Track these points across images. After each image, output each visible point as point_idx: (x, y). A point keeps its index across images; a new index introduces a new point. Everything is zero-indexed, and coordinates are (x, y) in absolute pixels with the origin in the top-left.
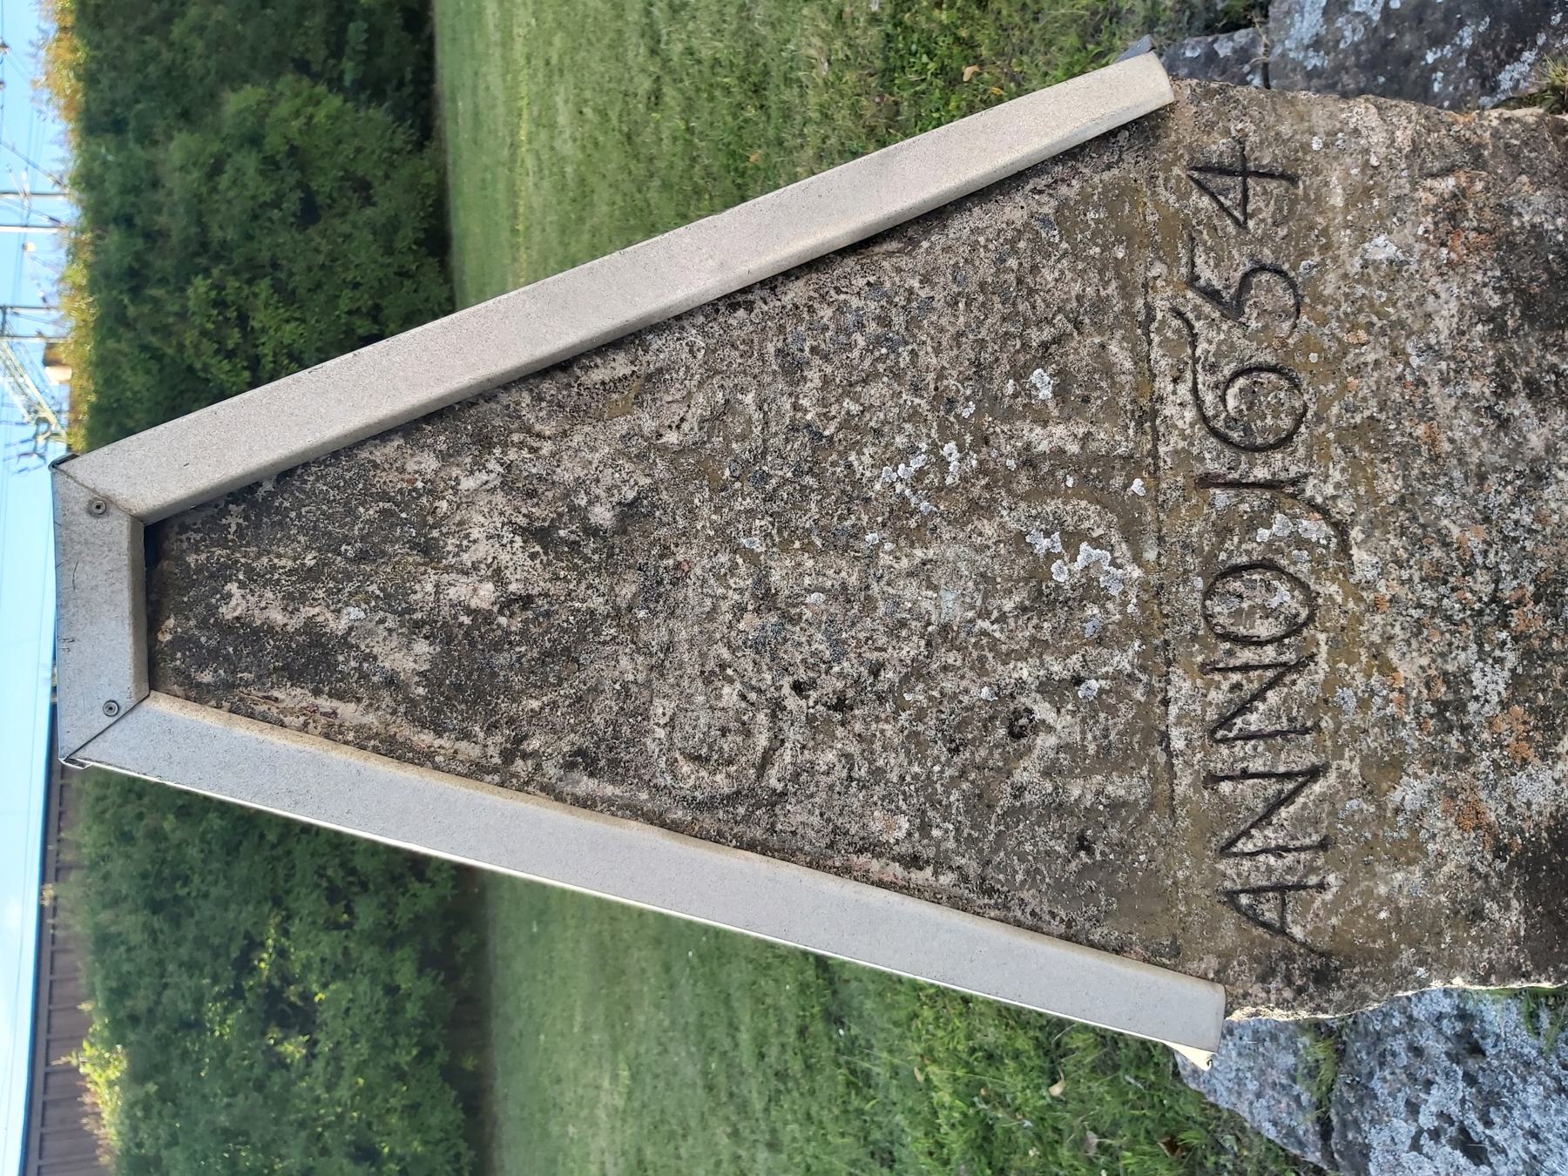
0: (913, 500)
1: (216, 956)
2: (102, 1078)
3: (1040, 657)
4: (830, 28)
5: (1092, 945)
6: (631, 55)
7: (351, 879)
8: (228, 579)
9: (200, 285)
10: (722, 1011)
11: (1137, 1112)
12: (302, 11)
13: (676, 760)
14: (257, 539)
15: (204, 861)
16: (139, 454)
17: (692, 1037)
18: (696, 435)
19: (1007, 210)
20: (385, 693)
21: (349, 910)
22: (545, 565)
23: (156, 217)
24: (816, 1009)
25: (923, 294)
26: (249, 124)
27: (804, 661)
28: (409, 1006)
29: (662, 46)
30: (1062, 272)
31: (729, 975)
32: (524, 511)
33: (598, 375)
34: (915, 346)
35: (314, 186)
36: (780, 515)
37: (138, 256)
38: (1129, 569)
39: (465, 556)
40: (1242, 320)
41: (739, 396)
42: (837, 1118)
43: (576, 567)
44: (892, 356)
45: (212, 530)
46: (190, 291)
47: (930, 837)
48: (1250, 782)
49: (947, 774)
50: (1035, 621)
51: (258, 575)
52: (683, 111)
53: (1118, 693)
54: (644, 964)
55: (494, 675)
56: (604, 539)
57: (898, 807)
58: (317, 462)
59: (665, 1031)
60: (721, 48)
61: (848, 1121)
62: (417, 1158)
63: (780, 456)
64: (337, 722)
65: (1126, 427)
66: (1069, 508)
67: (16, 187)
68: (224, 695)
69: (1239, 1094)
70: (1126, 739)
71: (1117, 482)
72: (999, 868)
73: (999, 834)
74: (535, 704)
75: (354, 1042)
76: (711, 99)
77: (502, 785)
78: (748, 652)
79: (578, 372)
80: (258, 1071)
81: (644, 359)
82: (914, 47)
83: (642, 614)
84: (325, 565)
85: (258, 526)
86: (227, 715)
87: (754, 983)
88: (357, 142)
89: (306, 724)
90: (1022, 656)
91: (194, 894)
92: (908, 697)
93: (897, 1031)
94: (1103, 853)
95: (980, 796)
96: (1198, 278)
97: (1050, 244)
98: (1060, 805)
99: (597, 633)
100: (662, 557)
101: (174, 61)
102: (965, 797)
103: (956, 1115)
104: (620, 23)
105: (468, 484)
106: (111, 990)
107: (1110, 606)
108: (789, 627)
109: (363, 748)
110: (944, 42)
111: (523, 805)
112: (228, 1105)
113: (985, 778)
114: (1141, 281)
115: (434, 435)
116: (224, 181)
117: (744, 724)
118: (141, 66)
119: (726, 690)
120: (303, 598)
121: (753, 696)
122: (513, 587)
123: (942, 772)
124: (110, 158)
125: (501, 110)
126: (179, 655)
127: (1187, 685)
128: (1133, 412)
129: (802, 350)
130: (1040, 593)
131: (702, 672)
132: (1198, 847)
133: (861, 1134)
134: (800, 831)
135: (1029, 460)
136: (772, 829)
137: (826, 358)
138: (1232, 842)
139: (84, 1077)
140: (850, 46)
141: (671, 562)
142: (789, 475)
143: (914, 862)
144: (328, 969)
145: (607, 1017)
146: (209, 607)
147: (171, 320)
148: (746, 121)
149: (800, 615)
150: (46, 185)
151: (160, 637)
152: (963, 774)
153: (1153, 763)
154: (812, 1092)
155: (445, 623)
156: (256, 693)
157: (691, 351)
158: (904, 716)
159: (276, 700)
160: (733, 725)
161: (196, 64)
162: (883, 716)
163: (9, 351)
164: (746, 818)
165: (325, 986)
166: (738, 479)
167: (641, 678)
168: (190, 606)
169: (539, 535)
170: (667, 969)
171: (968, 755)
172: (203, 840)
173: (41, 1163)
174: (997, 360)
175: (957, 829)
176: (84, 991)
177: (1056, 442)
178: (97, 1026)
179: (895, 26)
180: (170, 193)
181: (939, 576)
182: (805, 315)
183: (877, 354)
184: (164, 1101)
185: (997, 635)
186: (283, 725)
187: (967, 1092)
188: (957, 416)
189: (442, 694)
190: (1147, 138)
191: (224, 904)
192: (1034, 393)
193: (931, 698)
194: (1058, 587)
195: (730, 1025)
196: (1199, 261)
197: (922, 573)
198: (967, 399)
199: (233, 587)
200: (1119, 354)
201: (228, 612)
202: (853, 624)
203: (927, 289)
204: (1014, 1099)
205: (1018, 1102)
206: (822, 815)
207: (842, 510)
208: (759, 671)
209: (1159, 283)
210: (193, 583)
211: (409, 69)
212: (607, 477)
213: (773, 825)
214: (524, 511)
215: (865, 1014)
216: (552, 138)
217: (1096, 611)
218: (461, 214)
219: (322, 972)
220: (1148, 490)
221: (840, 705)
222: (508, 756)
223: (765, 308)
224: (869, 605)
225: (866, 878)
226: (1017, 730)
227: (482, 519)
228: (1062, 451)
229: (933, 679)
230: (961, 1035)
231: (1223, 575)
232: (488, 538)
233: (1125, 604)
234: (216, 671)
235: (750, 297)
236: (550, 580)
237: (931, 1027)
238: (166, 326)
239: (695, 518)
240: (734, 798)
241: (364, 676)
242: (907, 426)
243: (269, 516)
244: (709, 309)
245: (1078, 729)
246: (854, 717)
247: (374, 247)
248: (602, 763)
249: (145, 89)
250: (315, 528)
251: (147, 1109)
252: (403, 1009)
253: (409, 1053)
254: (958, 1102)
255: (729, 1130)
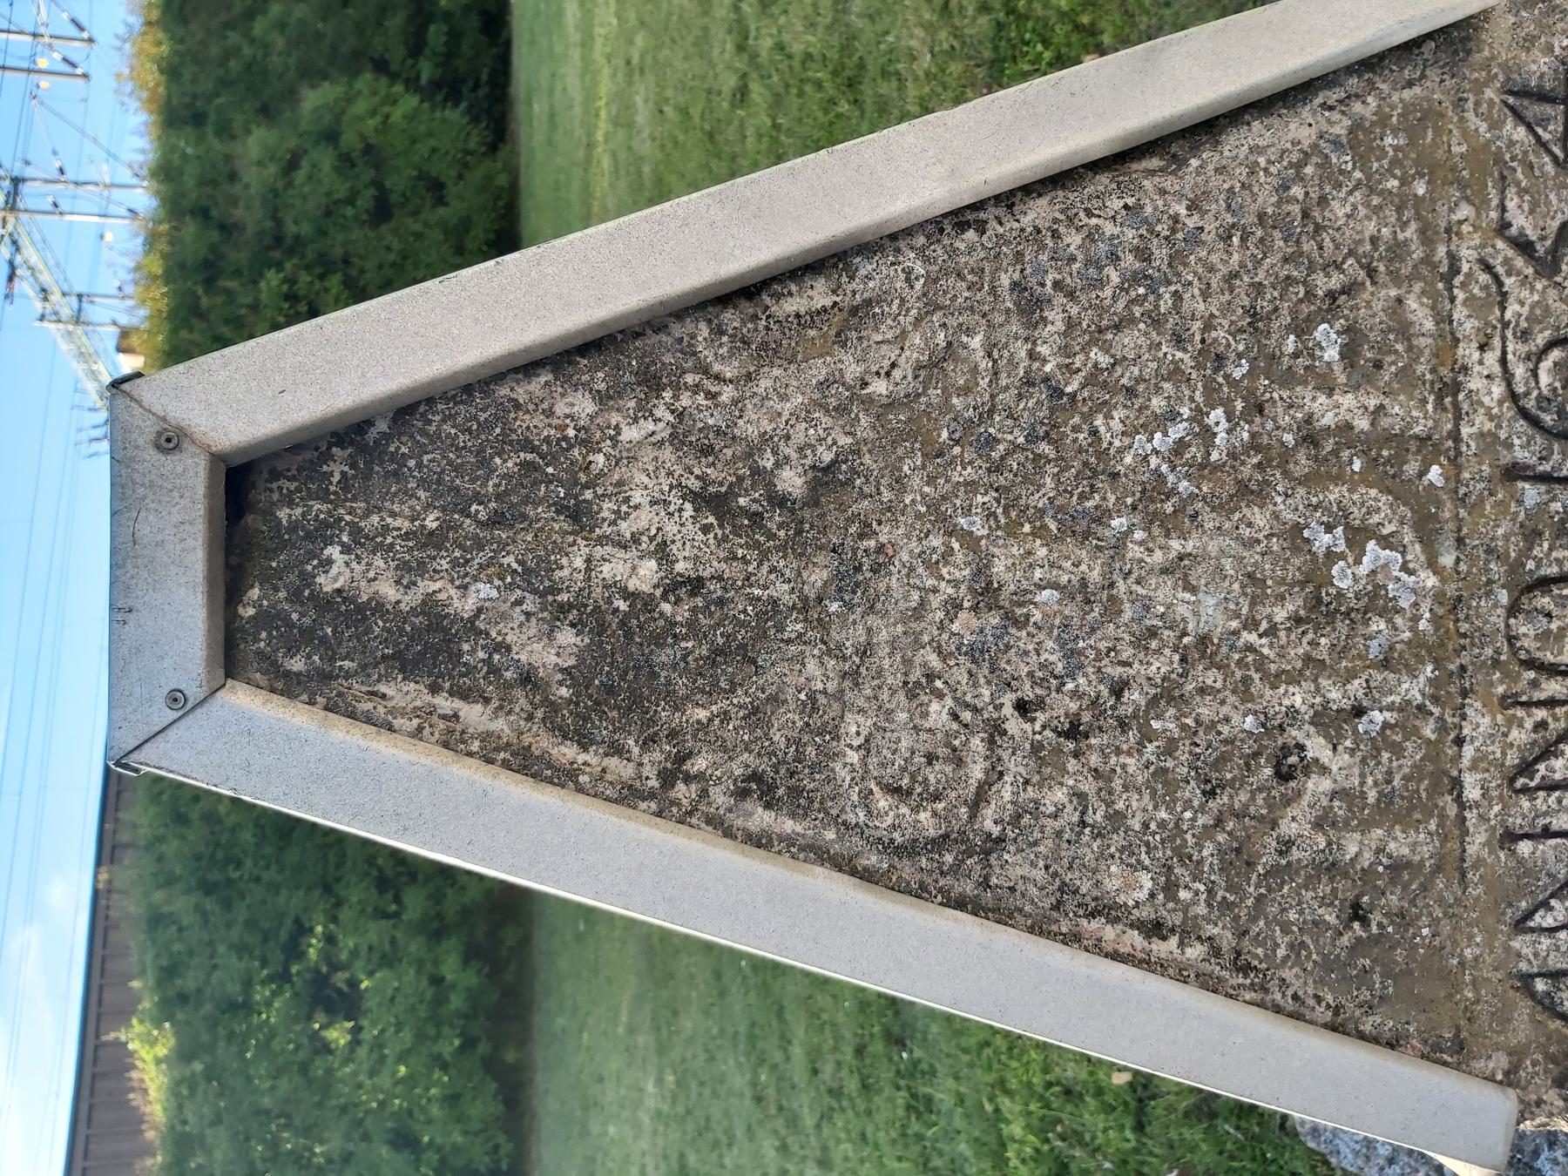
0: (1171, 478)
1: (266, 939)
2: (150, 1054)
3: (1315, 681)
4: (935, 18)
5: (1362, 1036)
6: (716, 51)
7: (400, 869)
8: (329, 541)
9: (272, 279)
10: (774, 1023)
11: (1235, 1164)
12: (383, 11)
13: (871, 792)
14: (366, 494)
15: (257, 845)
16: (223, 375)
17: (742, 1047)
18: (911, 385)
19: (1292, 126)
20: (518, 693)
21: (397, 899)
22: (720, 541)
23: (232, 210)
24: (876, 1029)
25: (1191, 223)
26: (326, 121)
27: (1031, 674)
28: (453, 997)
29: (751, 42)
30: (1354, 207)
31: (783, 987)
32: (697, 471)
33: (791, 306)
34: (1179, 287)
35: (388, 184)
36: (1007, 489)
37: (213, 248)
38: (1423, 575)
39: (623, 525)
40: (1558, 279)
41: (965, 339)
42: (894, 1142)
43: (757, 545)
44: (1151, 298)
45: (310, 479)
46: (263, 285)
47: (1176, 900)
48: (1553, 842)
49: (1200, 822)
50: (1310, 636)
51: (367, 537)
52: (770, 107)
53: (1404, 728)
54: (693, 970)
55: (654, 675)
56: (793, 511)
57: (1139, 861)
58: (445, 397)
59: (714, 1038)
60: (811, 41)
61: (906, 1146)
62: (456, 1149)
63: (1010, 416)
64: (459, 728)
65: (1424, 401)
66: (1355, 497)
67: (96, 178)
68: (314, 687)
69: (1368, 1158)
70: (1412, 786)
71: (1411, 468)
72: (1256, 940)
73: (1260, 899)
74: (702, 714)
75: (397, 1032)
76: (801, 94)
77: (659, 814)
78: (962, 659)
79: (767, 300)
80: (302, 1055)
81: (849, 288)
82: (1028, 36)
83: (834, 607)
84: (450, 528)
85: (367, 477)
86: (323, 713)
87: (810, 997)
88: (432, 142)
89: (420, 729)
90: (1294, 678)
91: (246, 877)
92: (1155, 724)
93: (965, 1058)
94: (1380, 925)
95: (1238, 851)
96: (1510, 225)
97: (1342, 172)
98: (1333, 864)
99: (780, 628)
100: (861, 536)
101: (254, 57)
102: (1221, 851)
103: (1028, 1150)
104: (706, 20)
105: (630, 434)
106: (162, 969)
107: (1399, 620)
108: (1013, 631)
109: (490, 761)
110: (1061, 30)
111: (685, 842)
112: (273, 1088)
113: (1245, 829)
114: (1443, 225)
115: (593, 369)
116: (300, 176)
117: (954, 750)
118: (223, 61)
119: (935, 707)
120: (421, 569)
121: (967, 716)
122: (680, 567)
123: (1194, 819)
124: (189, 151)
125: (578, 110)
126: (264, 635)
127: (1487, 720)
128: (1432, 383)
129: (1043, 285)
130: (1319, 601)
131: (906, 683)
132: (1491, 921)
133: (921, 1160)
134: (1020, 887)
135: (1310, 437)
136: (985, 884)
137: (1071, 295)
138: (1530, 915)
139: (131, 1054)
140: (956, 37)
141: (872, 543)
142: (1021, 440)
143: (1155, 929)
144: (375, 958)
145: (653, 1020)
146: (302, 573)
147: (243, 311)
148: (839, 116)
149: (1028, 616)
150: (125, 176)
151: (241, 610)
152: (1219, 822)
153: (1442, 817)
154: (869, 1113)
155: (597, 608)
156: (358, 687)
157: (908, 280)
158: (1150, 748)
159: (384, 696)
160: (942, 751)
161: (275, 59)
162: (1125, 747)
163: (84, 339)
164: (952, 869)
165: (371, 974)
166: (957, 442)
167: (832, 687)
168: (279, 574)
169: (713, 502)
170: (718, 976)
171: (1225, 799)
172: (257, 825)
173: (87, 1164)
174: (1276, 309)
175: (1210, 891)
176: (135, 969)
177: (1344, 415)
178: (146, 1004)
179: (1007, 14)
180: (247, 186)
181: (1199, 575)
182: (1049, 242)
183: (1133, 294)
184: (209, 1080)
185: (1266, 651)
186: (391, 729)
187: (1043, 1128)
188: (1227, 377)
189: (590, 697)
190: (1456, 52)
191: (274, 888)
192: (1318, 353)
193: (1184, 727)
194: (1340, 594)
195: (783, 1037)
196: (1511, 205)
197: (1178, 569)
198: (1240, 356)
199: (334, 551)
200: (1419, 312)
201: (327, 583)
202: (1093, 630)
203: (1196, 217)
204: (1094, 1138)
205: (1098, 1141)
206: (1047, 867)
207: (1084, 487)
208: (975, 685)
209: (1466, 228)
210: (285, 545)
211: (486, 70)
212: (799, 437)
213: (986, 878)
214: (697, 471)
215: (930, 1037)
216: (630, 138)
217: (1383, 626)
218: (533, 216)
219: (369, 960)
220: (1447, 479)
221: (1074, 731)
222: (667, 779)
223: (1001, 230)
224: (1113, 608)
225: (1097, 948)
226: (1284, 770)
227: (646, 480)
228: (1349, 427)
229: (1187, 703)
230: (1035, 1067)
231: (1530, 588)
232: (653, 503)
233: (1416, 619)
234: (309, 657)
235: (982, 216)
236: (726, 560)
237: (1003, 1057)
238: (239, 318)
239: (903, 490)
240: (940, 843)
241: (494, 671)
242: (1167, 386)
243: (381, 464)
244: (931, 228)
245: (1356, 771)
246: (1090, 747)
247: (445, 247)
248: (781, 792)
249: (225, 83)
250: (439, 482)
251: (193, 1089)
252: (447, 1000)
253: (451, 1043)
254: (1031, 1138)
255: (777, 1143)
